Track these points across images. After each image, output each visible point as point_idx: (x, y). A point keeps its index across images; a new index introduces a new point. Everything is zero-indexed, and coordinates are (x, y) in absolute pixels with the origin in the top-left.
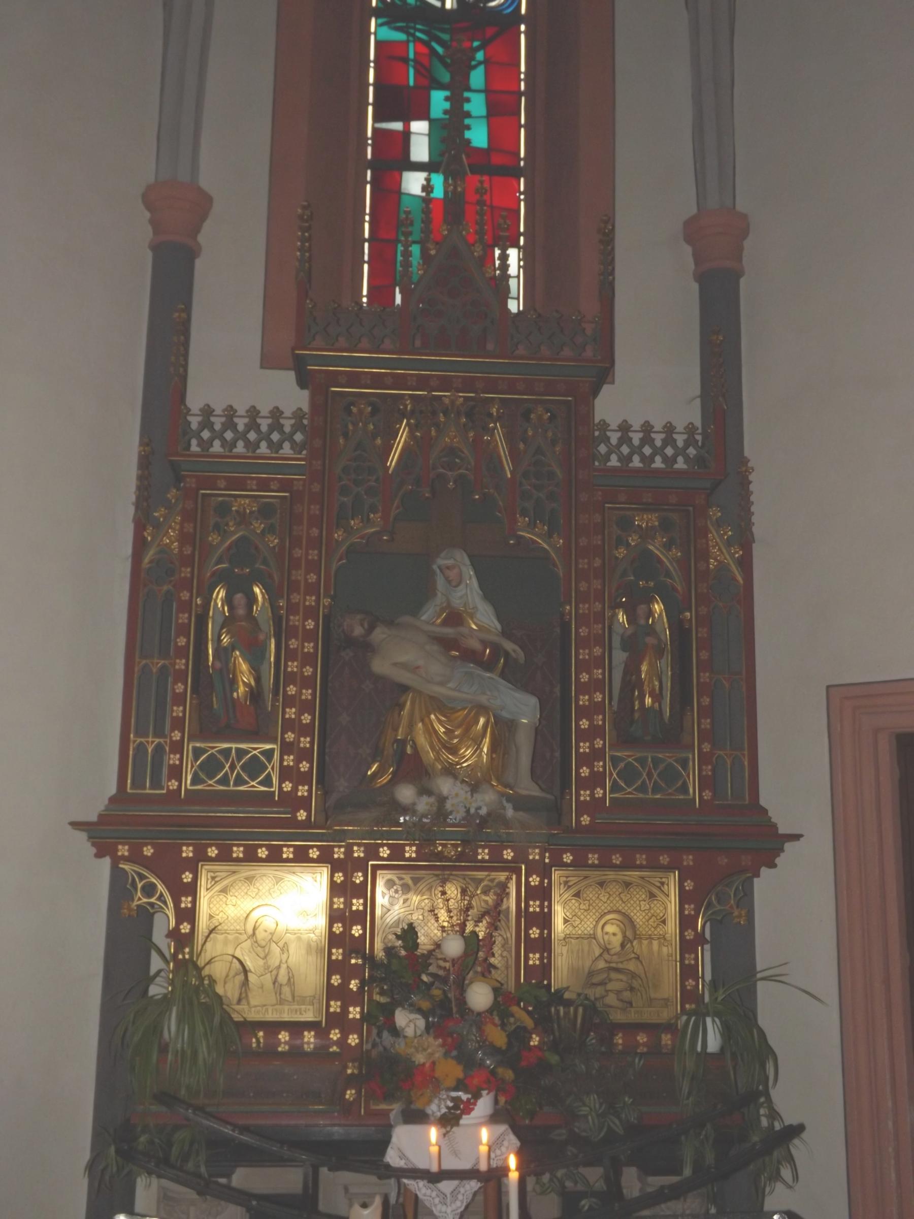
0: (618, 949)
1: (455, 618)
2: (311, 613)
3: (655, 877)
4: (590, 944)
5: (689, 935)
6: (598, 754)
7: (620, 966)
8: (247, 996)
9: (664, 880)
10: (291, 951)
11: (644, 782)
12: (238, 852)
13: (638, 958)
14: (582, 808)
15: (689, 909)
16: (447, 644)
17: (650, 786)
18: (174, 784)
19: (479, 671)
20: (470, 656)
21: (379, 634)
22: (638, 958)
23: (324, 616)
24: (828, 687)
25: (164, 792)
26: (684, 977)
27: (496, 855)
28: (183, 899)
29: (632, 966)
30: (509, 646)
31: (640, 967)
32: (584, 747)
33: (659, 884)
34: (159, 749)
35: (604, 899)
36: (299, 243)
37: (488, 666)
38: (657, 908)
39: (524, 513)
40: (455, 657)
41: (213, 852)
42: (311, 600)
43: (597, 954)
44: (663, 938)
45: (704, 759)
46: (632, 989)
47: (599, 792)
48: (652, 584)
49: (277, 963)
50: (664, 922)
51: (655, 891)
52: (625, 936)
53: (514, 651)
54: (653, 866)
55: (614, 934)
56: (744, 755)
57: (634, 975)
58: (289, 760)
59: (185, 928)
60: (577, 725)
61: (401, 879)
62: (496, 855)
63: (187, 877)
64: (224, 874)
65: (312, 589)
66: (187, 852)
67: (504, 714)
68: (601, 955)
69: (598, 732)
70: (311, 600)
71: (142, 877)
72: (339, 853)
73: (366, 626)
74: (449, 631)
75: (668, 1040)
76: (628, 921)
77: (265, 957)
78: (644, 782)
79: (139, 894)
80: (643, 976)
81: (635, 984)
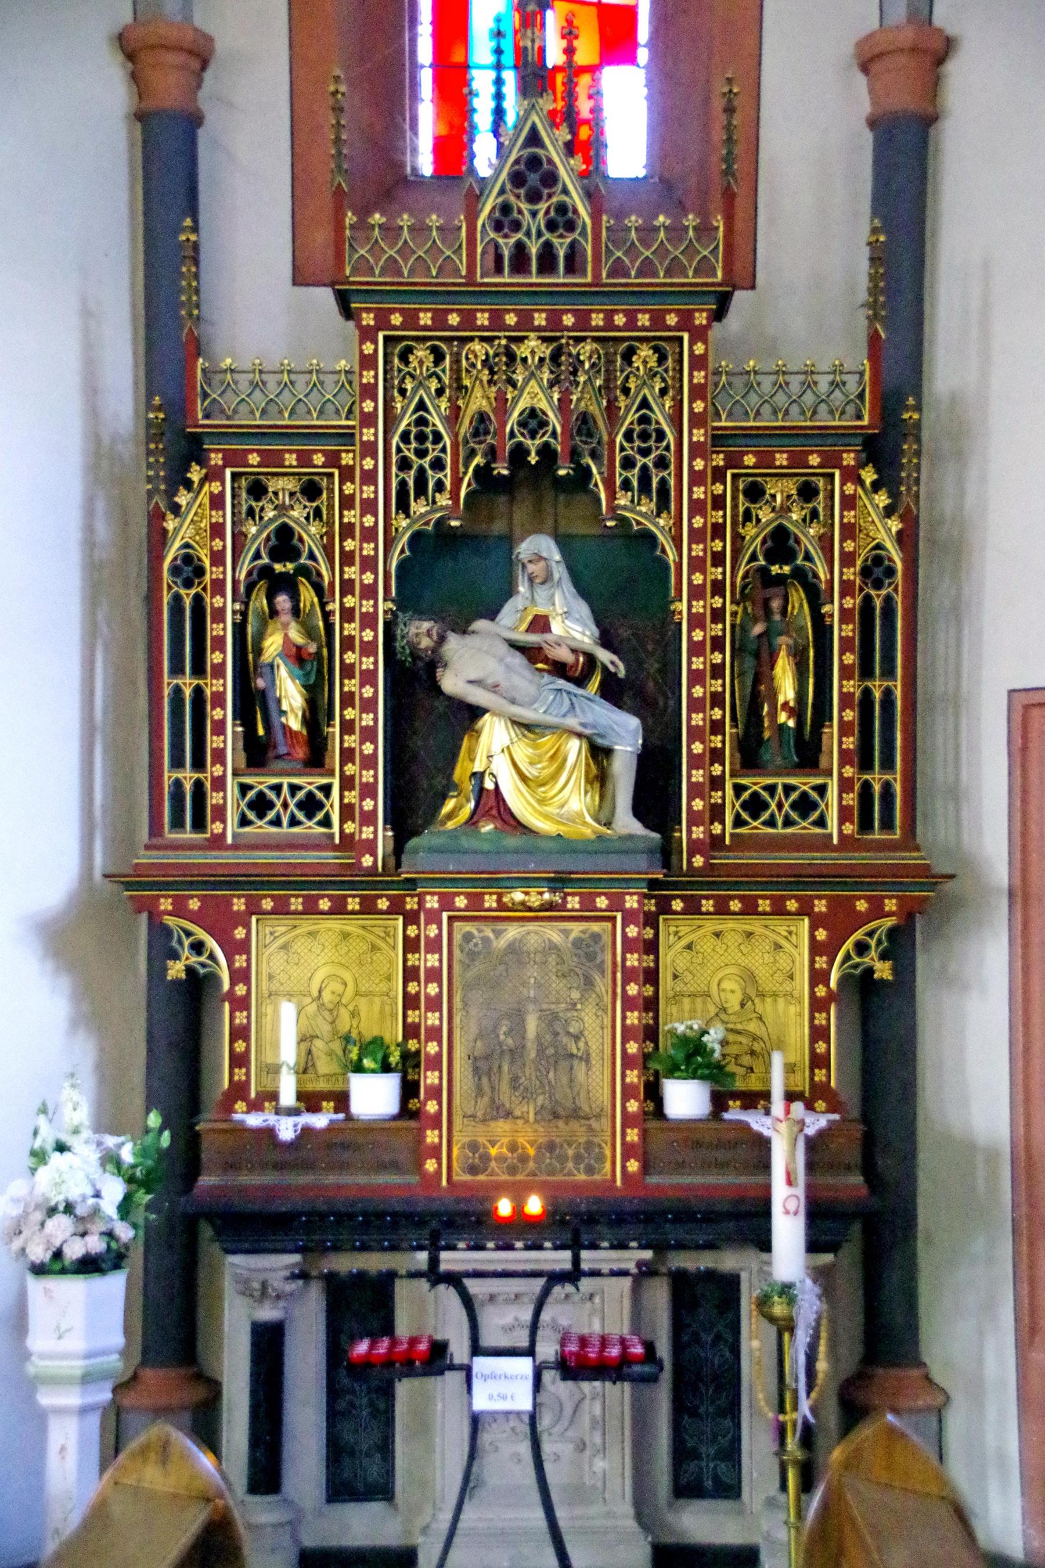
0: (737, 1007)
1: (540, 624)
2: (368, 621)
3: (780, 926)
4: (704, 1003)
5: (821, 991)
6: (717, 783)
7: (739, 1027)
8: (314, 1065)
9: (792, 928)
10: (363, 1014)
11: (772, 815)
12: (296, 904)
13: (760, 1018)
14: (695, 847)
15: (821, 962)
16: (531, 653)
17: (780, 821)
18: (218, 828)
19: (570, 687)
20: (559, 669)
21: (454, 643)
22: (760, 1018)
23: (385, 623)
24: (1011, 692)
25: (208, 835)
26: (813, 1041)
27: (588, 903)
28: (237, 957)
29: (753, 1027)
30: (604, 656)
31: (763, 1028)
32: (698, 775)
33: (785, 934)
34: (198, 785)
35: (343, 952)
36: (344, 137)
37: (581, 681)
38: (783, 961)
39: (626, 485)
40: (540, 670)
41: (267, 904)
42: (367, 606)
43: (712, 1014)
44: (789, 996)
45: (845, 785)
46: (753, 1053)
47: (717, 828)
48: (787, 569)
49: (347, 1029)
50: (791, 977)
51: (783, 942)
52: (744, 993)
53: (613, 663)
54: (779, 910)
55: (732, 991)
56: (895, 779)
57: (755, 1038)
58: (352, 797)
59: (240, 990)
60: (689, 750)
61: (480, 931)
62: (588, 903)
63: (240, 933)
64: (283, 929)
65: (369, 592)
66: (239, 905)
67: (600, 741)
68: (717, 1015)
69: (717, 756)
70: (367, 606)
71: (188, 934)
72: (411, 904)
73: (435, 637)
74: (533, 638)
75: (788, 1112)
76: (749, 977)
77: (333, 1022)
78: (772, 815)
79: (866, 960)
80: (766, 1038)
81: (757, 1047)
